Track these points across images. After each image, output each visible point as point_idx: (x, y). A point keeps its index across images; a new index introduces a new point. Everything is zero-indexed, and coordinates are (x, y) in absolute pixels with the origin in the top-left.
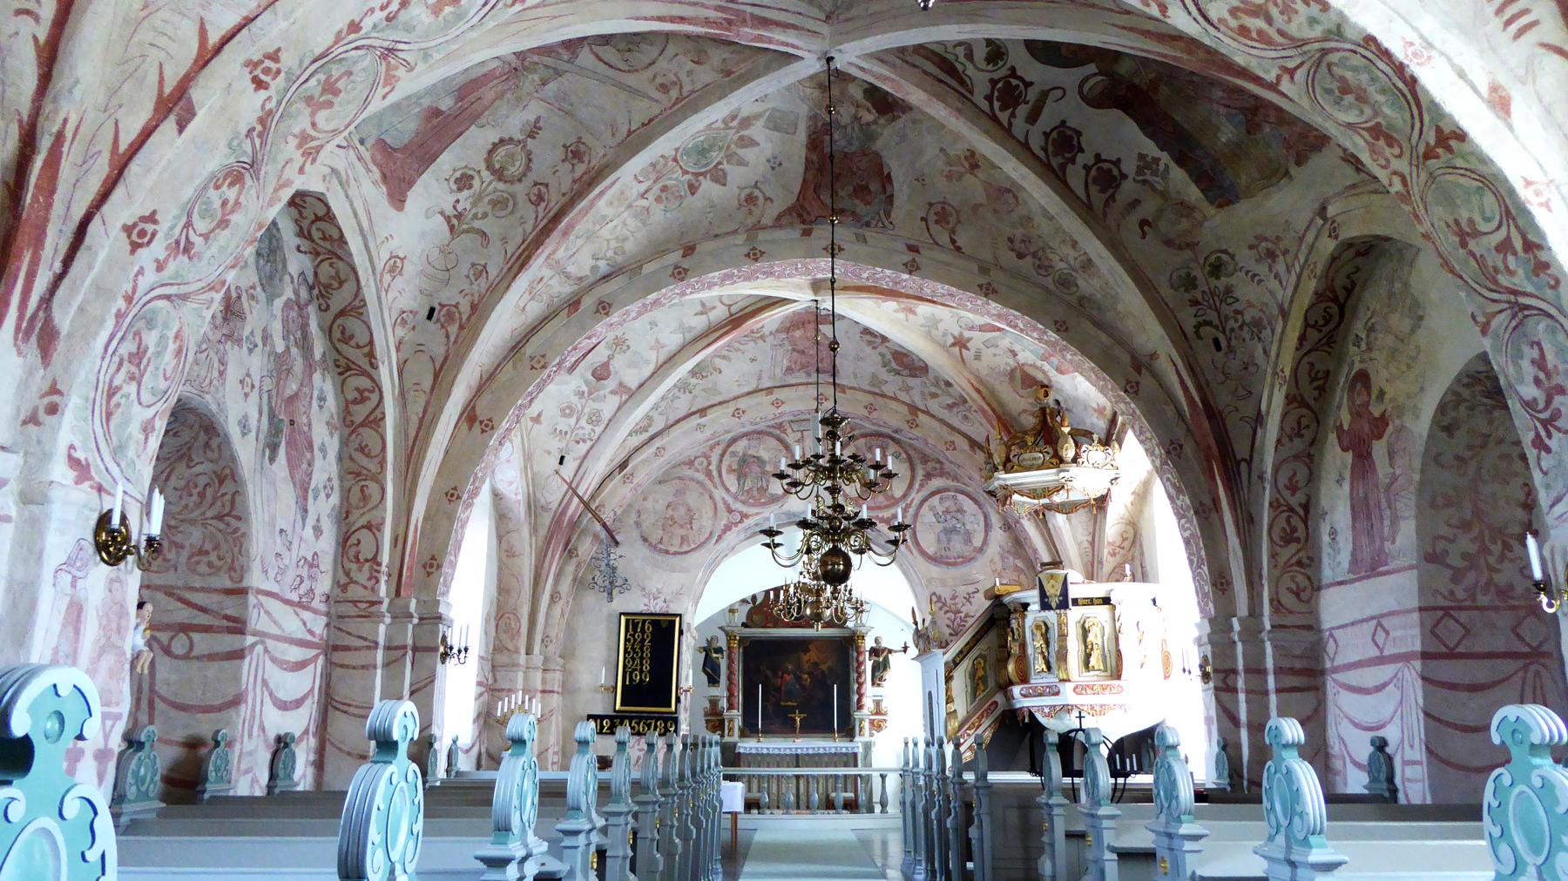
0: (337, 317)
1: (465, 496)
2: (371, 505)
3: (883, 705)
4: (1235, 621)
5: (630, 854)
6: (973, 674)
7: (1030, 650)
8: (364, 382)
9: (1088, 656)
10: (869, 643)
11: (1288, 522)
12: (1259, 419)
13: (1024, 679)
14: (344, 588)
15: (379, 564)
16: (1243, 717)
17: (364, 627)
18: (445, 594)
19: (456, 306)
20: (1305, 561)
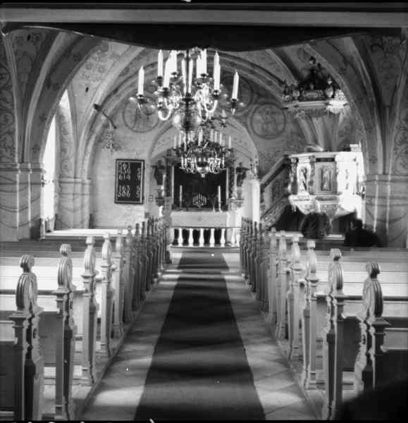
1: (48, 118)
6: (273, 189)
7: (298, 181)
9: (322, 185)
10: (236, 165)
13: (295, 192)
15: (14, 148)
18: (55, 196)
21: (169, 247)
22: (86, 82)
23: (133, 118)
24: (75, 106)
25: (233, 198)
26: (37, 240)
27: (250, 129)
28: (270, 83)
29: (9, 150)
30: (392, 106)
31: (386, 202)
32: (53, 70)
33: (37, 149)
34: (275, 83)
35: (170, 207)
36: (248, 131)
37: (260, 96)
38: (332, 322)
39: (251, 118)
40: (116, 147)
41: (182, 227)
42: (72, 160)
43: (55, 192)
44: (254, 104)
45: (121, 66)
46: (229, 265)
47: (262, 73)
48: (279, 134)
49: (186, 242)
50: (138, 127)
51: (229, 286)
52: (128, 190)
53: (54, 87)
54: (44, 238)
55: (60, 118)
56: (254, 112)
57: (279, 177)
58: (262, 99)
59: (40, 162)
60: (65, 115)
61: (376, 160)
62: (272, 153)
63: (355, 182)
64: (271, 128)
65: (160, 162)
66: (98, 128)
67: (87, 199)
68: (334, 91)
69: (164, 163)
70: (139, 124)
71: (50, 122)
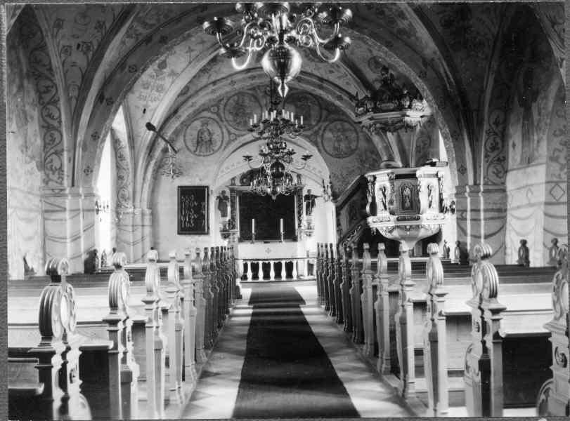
0: (32, 52)
1: (101, 137)
2: (55, 143)
3: (312, 225)
4: (467, 187)
5: (193, 299)
8: (49, 83)
10: (305, 193)
11: (494, 141)
12: (482, 91)
14: (47, 183)
15: (63, 171)
16: (469, 232)
17: (59, 201)
19: (91, 42)
20: (502, 158)
21: (238, 281)
22: (145, 103)
23: (195, 141)
24: (132, 128)
25: (303, 228)
26: (92, 273)
27: (321, 148)
28: (340, 98)
29: (57, 173)
30: (479, 110)
31: (480, 215)
32: (107, 82)
33: (89, 171)
34: (346, 98)
35: (236, 240)
36: (319, 150)
37: (330, 112)
38: (484, 343)
39: (323, 135)
40: (178, 173)
41: (250, 260)
42: (130, 189)
43: (112, 223)
44: (324, 121)
45: (180, 84)
46: (304, 298)
47: (331, 88)
48: (352, 152)
49: (255, 276)
50: (200, 151)
51: (309, 318)
52: (193, 223)
53: (107, 102)
54: (100, 271)
55: (116, 142)
56: (324, 130)
57: (355, 198)
58: (332, 116)
59: (93, 186)
60: (121, 140)
61: (466, 169)
62: (345, 173)
63: (516, 148)
64: (343, 145)
65: (224, 192)
66: (158, 153)
67: (147, 230)
68: (411, 101)
69: (228, 194)
70: (201, 148)
71: (104, 141)
